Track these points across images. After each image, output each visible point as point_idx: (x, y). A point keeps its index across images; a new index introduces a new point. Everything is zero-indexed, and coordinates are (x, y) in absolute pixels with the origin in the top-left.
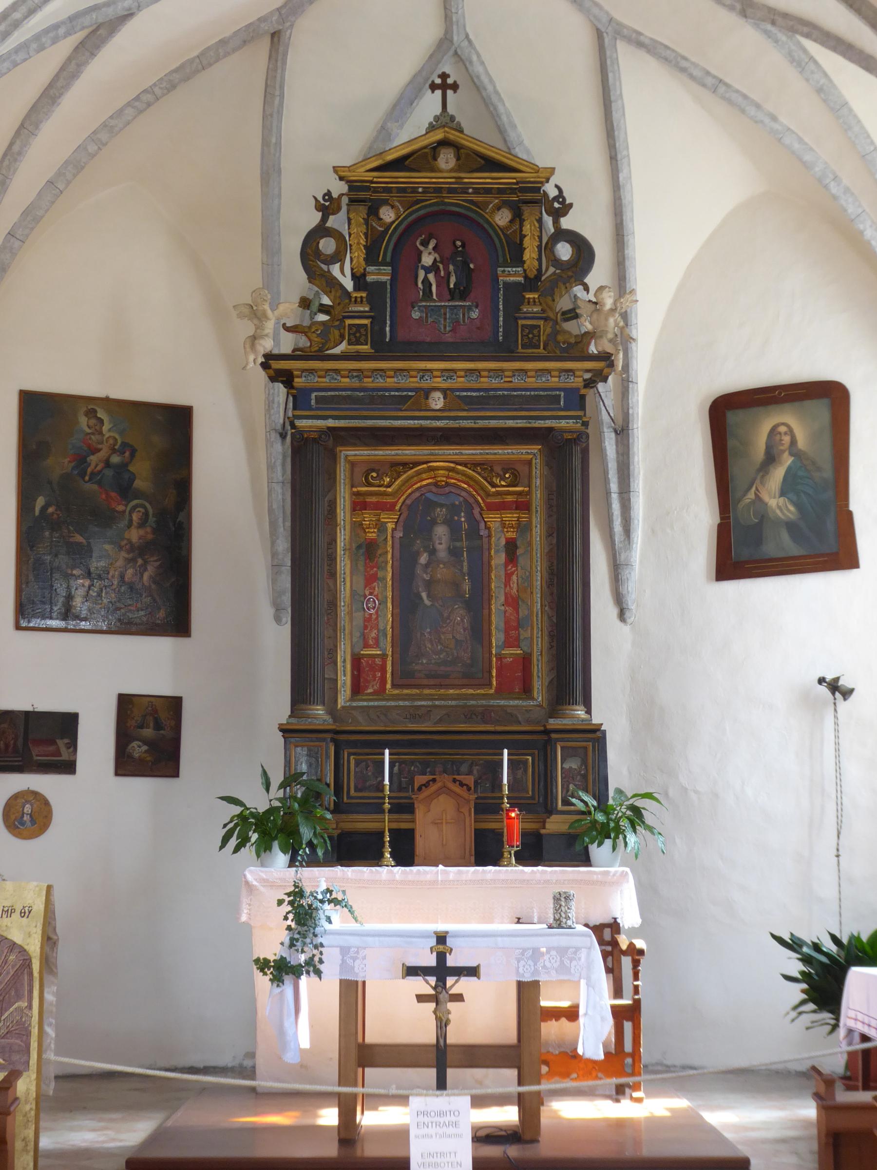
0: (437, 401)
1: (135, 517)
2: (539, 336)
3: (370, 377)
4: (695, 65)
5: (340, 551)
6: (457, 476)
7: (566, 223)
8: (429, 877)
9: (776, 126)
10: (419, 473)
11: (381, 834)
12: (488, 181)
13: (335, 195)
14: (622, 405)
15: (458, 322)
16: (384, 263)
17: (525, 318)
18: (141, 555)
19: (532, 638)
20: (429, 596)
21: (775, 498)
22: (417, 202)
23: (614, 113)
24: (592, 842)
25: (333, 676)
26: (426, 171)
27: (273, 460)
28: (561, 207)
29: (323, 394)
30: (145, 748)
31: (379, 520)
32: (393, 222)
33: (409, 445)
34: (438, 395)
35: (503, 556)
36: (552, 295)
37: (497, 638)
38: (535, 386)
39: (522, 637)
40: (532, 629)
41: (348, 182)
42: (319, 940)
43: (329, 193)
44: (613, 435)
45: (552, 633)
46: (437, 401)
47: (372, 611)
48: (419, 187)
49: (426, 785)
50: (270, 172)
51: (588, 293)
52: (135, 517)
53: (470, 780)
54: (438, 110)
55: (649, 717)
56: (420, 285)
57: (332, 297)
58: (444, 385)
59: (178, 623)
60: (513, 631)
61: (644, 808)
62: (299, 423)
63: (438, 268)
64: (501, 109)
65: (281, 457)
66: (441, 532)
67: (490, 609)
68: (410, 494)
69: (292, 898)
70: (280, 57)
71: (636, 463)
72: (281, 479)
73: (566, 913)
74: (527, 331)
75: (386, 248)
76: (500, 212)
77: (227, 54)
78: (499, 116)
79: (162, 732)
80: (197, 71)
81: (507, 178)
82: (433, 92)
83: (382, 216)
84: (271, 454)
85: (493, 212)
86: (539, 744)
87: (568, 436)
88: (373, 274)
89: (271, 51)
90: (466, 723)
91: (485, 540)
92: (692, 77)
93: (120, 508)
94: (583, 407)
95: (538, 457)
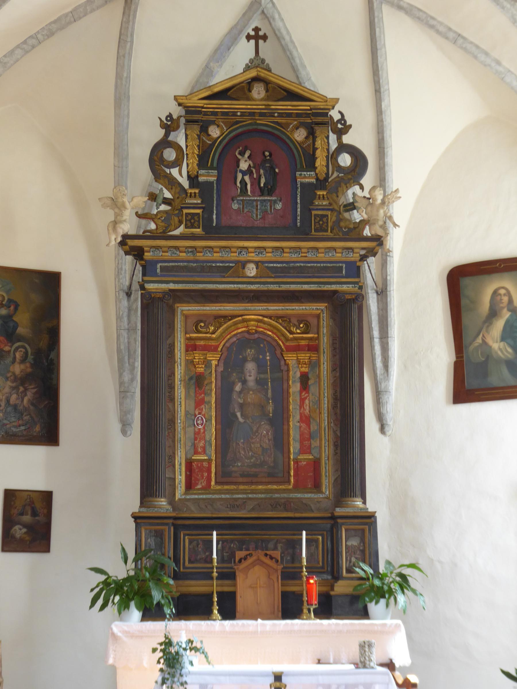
0: (251, 270)
1: (18, 355)
2: (327, 223)
3: (202, 252)
4: (441, 23)
5: (177, 382)
6: (264, 326)
7: (346, 139)
8: (251, 629)
9: (500, 69)
10: (236, 324)
11: (210, 596)
12: (289, 107)
13: (175, 117)
14: (382, 274)
15: (266, 211)
16: (212, 168)
17: (317, 209)
18: (22, 383)
19: (320, 447)
20: (242, 415)
21: (497, 342)
22: (237, 123)
23: (379, 58)
24: (371, 601)
25: (173, 477)
26: (244, 100)
27: (121, 314)
28: (342, 128)
29: (166, 264)
30: (24, 530)
31: (206, 358)
32: (219, 137)
33: (229, 303)
34: (252, 266)
35: (298, 385)
36: (337, 192)
37: (294, 447)
38: (324, 259)
39: (313, 446)
40: (321, 440)
41: (185, 107)
42: (184, 679)
43: (170, 115)
44: (375, 295)
45: (336, 443)
46: (251, 270)
47: (200, 427)
48: (237, 112)
49: (245, 558)
50: (121, 98)
51: (363, 191)
52: (18, 355)
53: (277, 554)
54: (252, 55)
55: (404, 505)
56: (238, 184)
57: (173, 193)
58: (257, 259)
59: (50, 436)
60: (306, 440)
61: (409, 576)
62: (148, 286)
63: (252, 172)
64: (295, 54)
65: (127, 310)
66: (251, 367)
67: (289, 425)
68: (229, 339)
69: (163, 647)
70: (132, 13)
71: (392, 316)
72: (127, 327)
73: (369, 657)
74: (318, 219)
75: (214, 156)
76: (298, 131)
77: (92, 11)
78: (293, 58)
79: (37, 518)
80: (70, 23)
81: (304, 106)
82: (248, 41)
83: (210, 133)
84: (119, 309)
85: (292, 131)
86: (330, 526)
87: (348, 297)
88: (203, 175)
89: (124, 8)
90: (272, 511)
91: (285, 373)
92: (438, 32)
93: (7, 348)
94: (358, 276)
95: (325, 312)
